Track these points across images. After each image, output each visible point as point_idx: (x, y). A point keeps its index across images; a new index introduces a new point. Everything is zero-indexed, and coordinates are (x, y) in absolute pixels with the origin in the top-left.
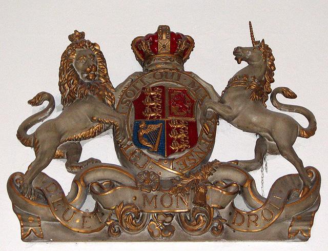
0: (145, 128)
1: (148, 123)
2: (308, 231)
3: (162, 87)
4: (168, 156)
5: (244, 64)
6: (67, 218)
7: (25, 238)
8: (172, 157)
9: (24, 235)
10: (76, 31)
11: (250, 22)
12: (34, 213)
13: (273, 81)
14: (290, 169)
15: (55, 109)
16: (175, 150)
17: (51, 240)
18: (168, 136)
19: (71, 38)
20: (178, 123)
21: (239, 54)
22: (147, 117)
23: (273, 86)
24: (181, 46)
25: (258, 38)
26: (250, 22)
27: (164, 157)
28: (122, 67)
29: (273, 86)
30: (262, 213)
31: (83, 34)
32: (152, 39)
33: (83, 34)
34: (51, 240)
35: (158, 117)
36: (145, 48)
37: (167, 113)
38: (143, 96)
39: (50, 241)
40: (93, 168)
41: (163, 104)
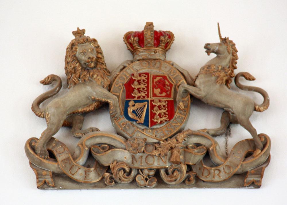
0: (134, 106)
1: (136, 102)
2: (260, 182)
3: (147, 74)
4: (151, 126)
5: (213, 55)
6: (73, 173)
7: (43, 185)
8: (154, 127)
9: (153, 122)
10: (150, 25)
11: (218, 23)
12: (47, 168)
13: (235, 68)
14: (248, 135)
15: (62, 87)
16: (157, 122)
17: (61, 188)
18: (151, 112)
19: (74, 33)
20: (160, 101)
21: (208, 49)
22: (134, 97)
23: (236, 72)
24: (162, 40)
25: (223, 37)
26: (218, 23)
27: (148, 126)
28: (115, 55)
29: (236, 72)
30: (224, 169)
31: (83, 31)
32: (140, 37)
33: (83, 31)
34: (61, 188)
35: (144, 97)
36: (136, 41)
37: (151, 94)
38: (131, 81)
39: (60, 189)
40: (93, 137)
41: (148, 87)
